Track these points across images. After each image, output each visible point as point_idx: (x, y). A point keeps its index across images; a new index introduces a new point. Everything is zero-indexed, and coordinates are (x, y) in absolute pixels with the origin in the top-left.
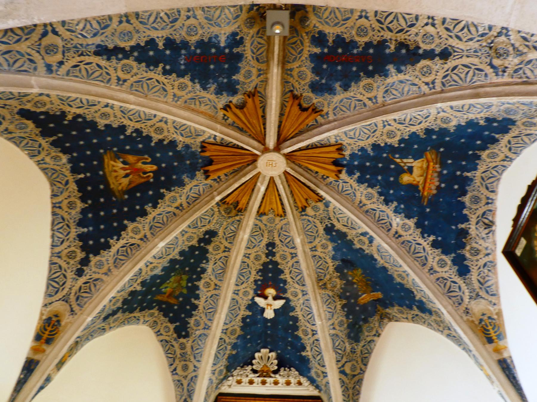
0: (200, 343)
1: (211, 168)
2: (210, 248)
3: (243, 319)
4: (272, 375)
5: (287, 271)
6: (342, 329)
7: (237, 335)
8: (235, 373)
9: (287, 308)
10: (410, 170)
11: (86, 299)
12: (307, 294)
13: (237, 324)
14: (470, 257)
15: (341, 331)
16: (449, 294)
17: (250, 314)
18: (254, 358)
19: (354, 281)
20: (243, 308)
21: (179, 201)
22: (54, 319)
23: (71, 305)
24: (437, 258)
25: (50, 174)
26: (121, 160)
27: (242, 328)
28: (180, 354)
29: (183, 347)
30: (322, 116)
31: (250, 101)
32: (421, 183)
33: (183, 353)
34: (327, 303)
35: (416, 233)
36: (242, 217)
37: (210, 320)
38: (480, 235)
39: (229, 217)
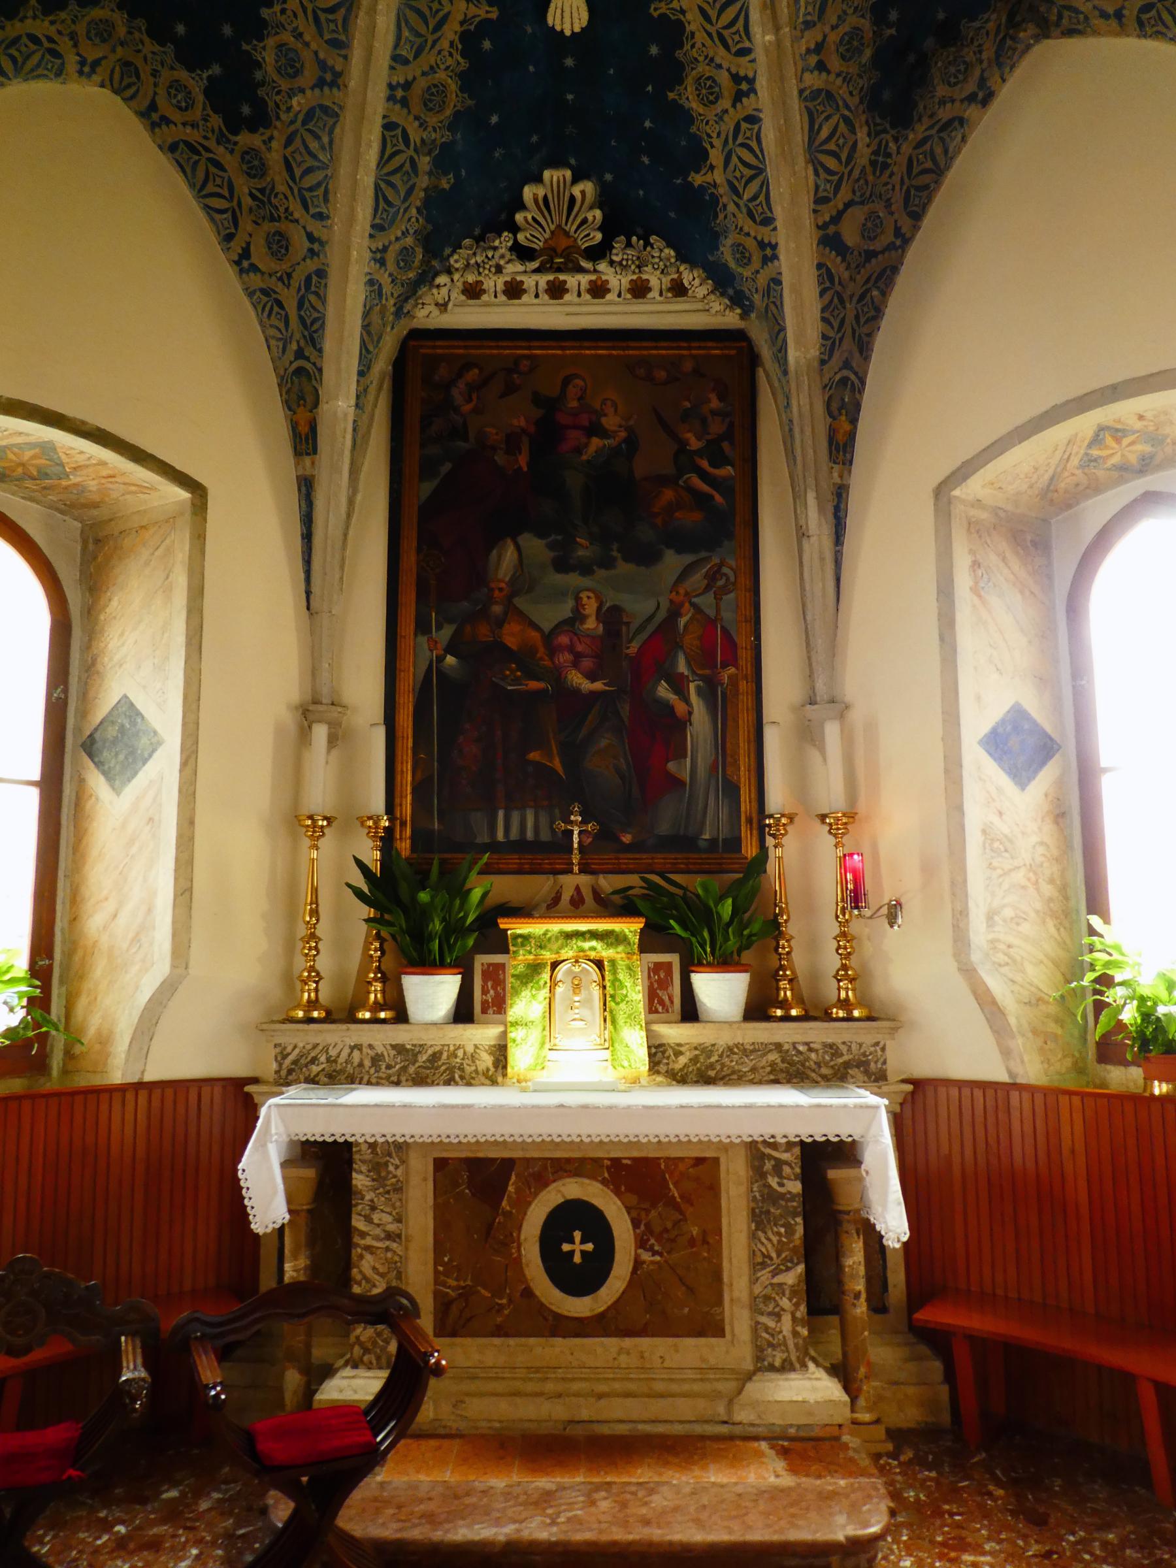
0: (314, 145)
3: (464, 36)
4: (584, 264)
7: (448, 112)
8: (456, 261)
13: (445, 61)
15: (847, 80)
17: (494, 15)
18: (522, 207)
27: (466, 81)
28: (251, 195)
29: (254, 165)
33: (262, 191)
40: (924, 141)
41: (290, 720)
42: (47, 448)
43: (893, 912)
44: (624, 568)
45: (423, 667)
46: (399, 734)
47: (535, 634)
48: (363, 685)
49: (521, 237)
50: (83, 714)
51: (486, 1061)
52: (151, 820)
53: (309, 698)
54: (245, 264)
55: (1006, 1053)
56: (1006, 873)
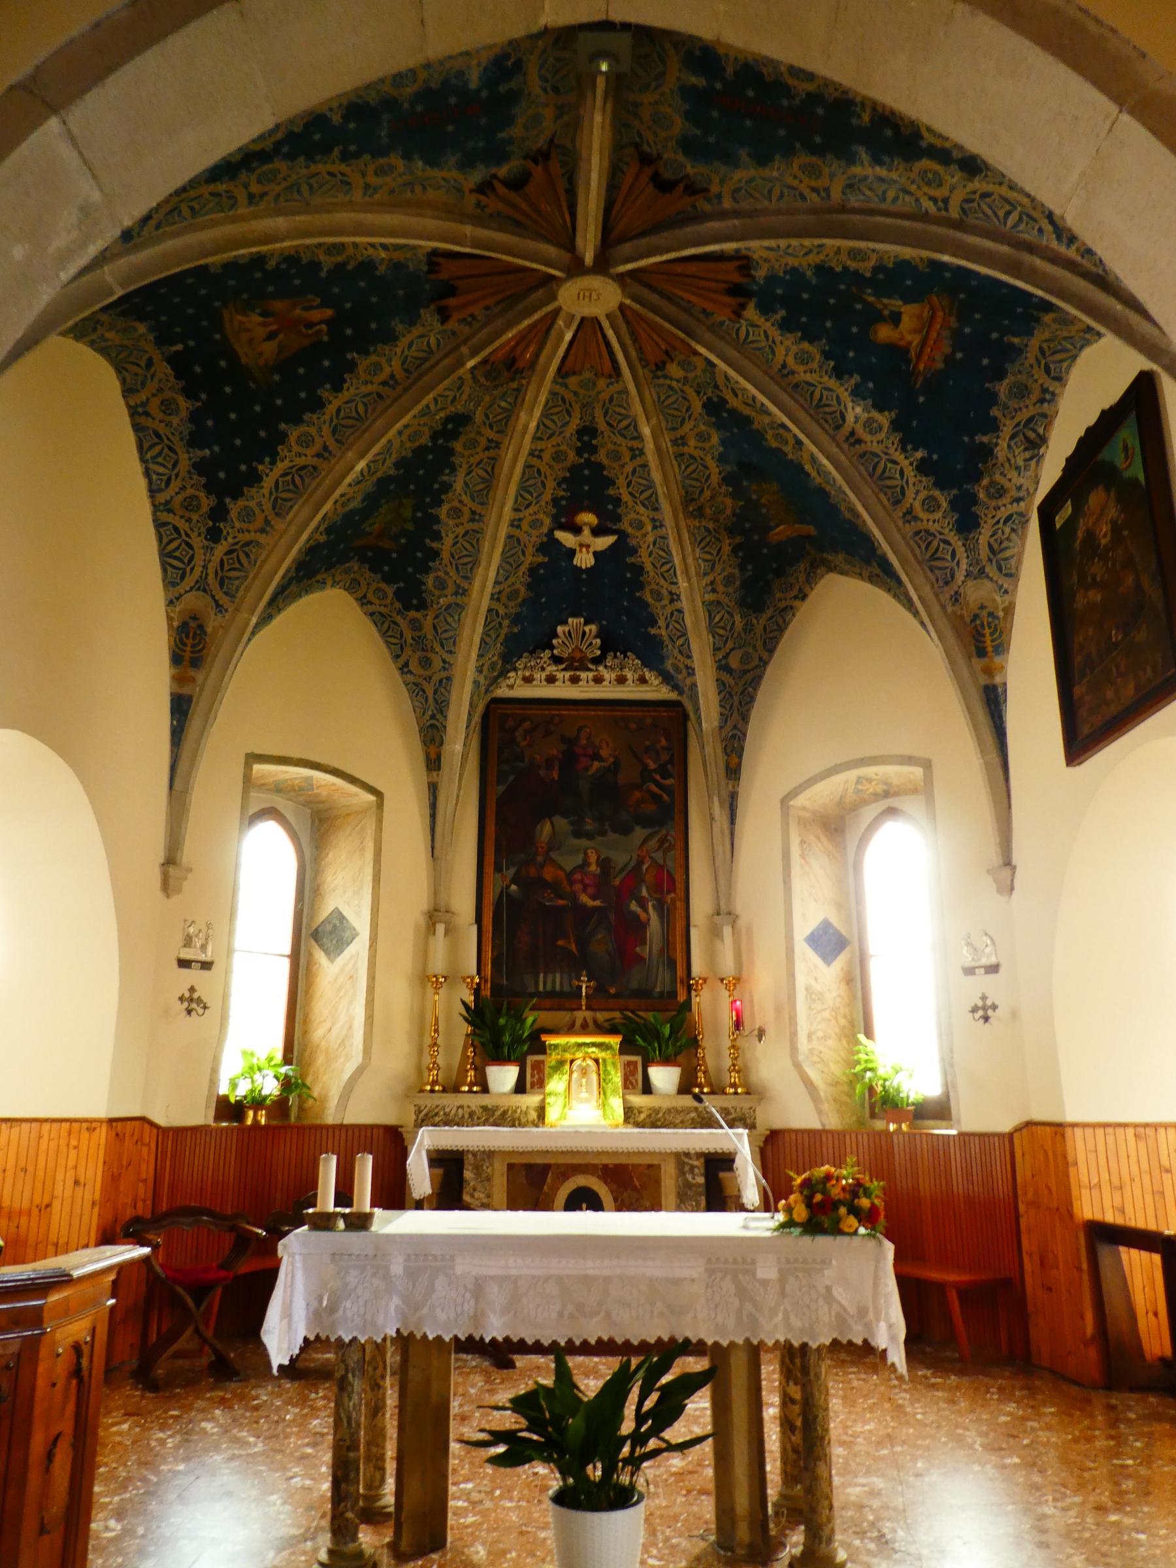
0: (450, 619)
1: (452, 302)
2: (458, 446)
4: (591, 666)
5: (621, 482)
6: (731, 590)
7: (520, 600)
8: (520, 665)
9: (622, 548)
10: (896, 318)
11: (236, 583)
12: (661, 526)
13: (520, 580)
14: (986, 500)
15: (728, 595)
16: (933, 563)
17: (546, 559)
18: (556, 636)
19: (763, 501)
20: (530, 550)
21: (387, 370)
22: (192, 624)
23: (213, 597)
24: (923, 495)
25: (114, 355)
26: (258, 311)
27: (529, 586)
29: (416, 625)
30: (709, 200)
31: (538, 171)
32: (914, 344)
34: (703, 544)
35: (892, 438)
36: (524, 382)
37: (465, 578)
38: (1013, 461)
39: (496, 387)
40: (772, 617)
41: (422, 920)
42: (309, 779)
43: (761, 1034)
44: (612, 836)
45: (498, 890)
46: (484, 929)
47: (561, 873)
48: (463, 901)
49: (555, 652)
50: (312, 917)
51: (533, 1115)
52: (351, 977)
53: (432, 908)
54: (405, 670)
55: (820, 1112)
56: (818, 1012)
